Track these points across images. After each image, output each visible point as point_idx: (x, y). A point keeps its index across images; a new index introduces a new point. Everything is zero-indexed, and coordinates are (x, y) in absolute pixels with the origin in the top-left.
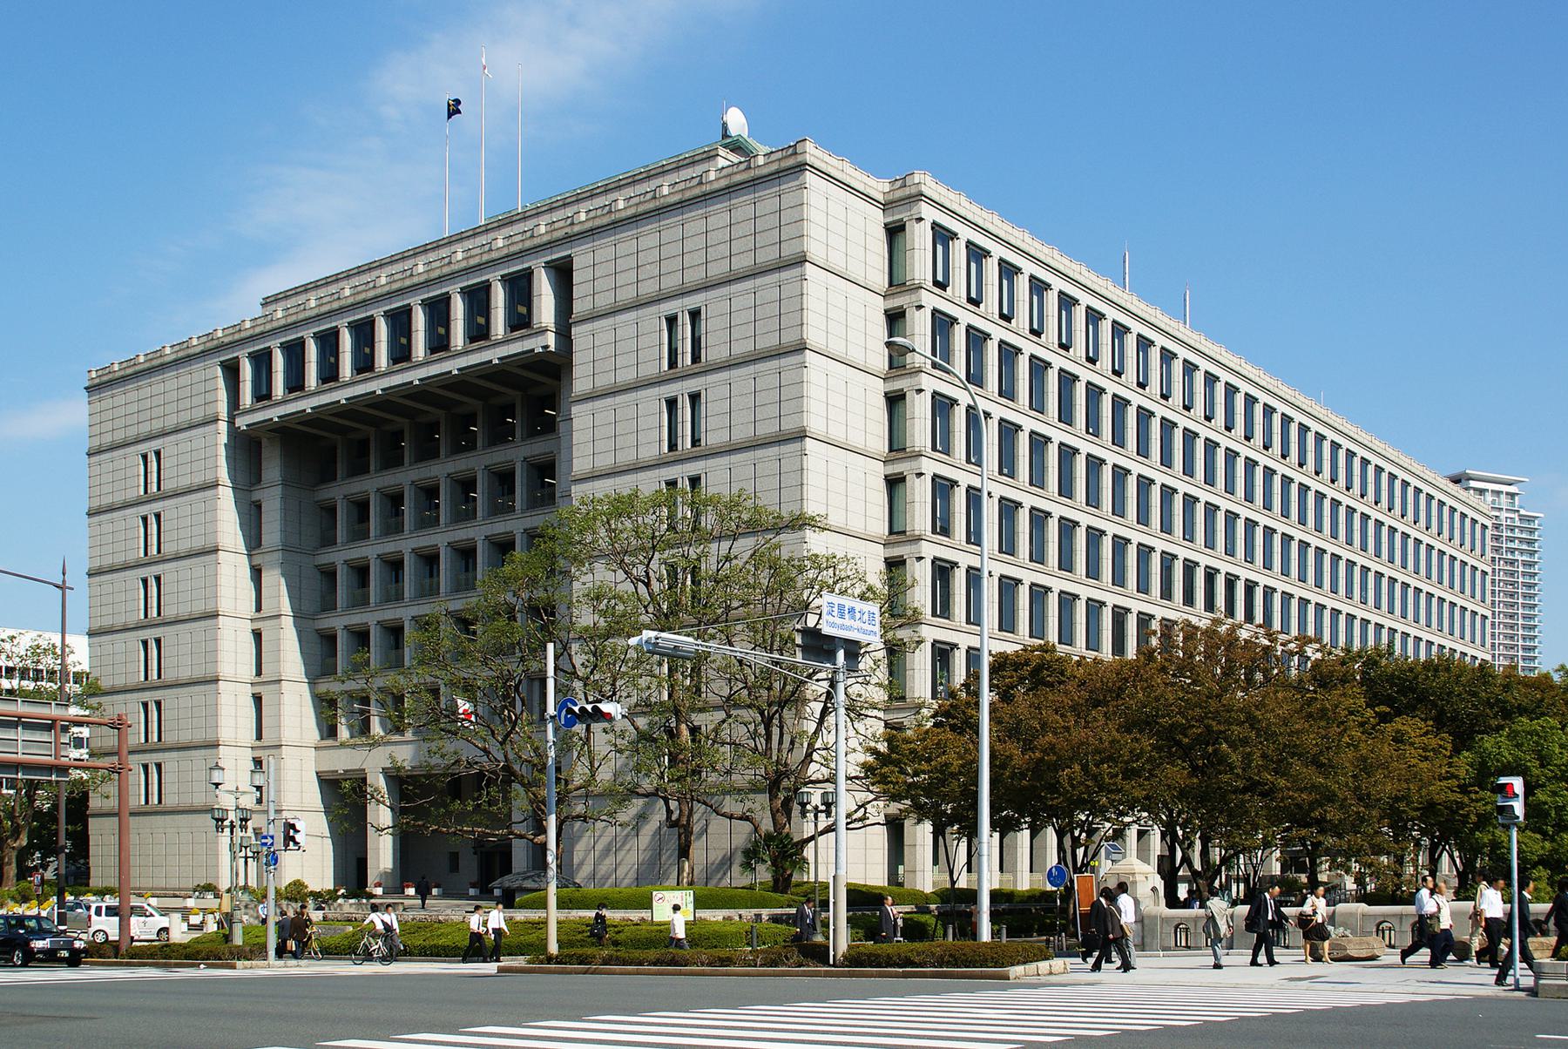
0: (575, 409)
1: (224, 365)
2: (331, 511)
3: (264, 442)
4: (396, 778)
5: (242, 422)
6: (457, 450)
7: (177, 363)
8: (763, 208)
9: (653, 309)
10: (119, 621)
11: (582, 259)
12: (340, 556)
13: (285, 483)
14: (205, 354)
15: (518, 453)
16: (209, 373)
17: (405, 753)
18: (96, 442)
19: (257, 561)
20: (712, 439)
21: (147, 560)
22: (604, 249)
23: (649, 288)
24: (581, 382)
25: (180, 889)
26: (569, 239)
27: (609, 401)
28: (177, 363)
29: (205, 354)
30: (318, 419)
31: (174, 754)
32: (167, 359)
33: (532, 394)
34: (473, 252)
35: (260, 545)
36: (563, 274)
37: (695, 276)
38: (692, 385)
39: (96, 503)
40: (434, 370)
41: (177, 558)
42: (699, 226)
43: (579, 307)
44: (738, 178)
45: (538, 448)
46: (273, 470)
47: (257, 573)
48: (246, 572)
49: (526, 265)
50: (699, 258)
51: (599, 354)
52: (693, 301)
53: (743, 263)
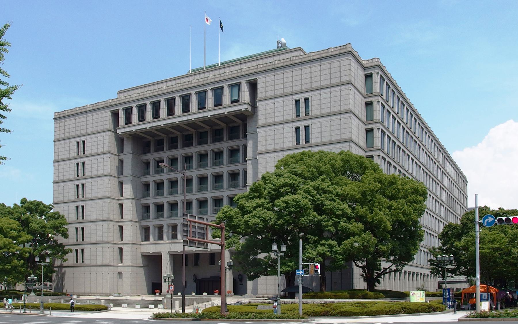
0: (258, 130)
1: (112, 112)
2: (148, 164)
3: (125, 139)
4: (175, 258)
5: (119, 131)
6: (231, 138)
7: (92, 111)
8: (94, 117)
9: (290, 97)
10: (66, 199)
11: (261, 81)
12: (152, 179)
13: (133, 153)
14: (104, 108)
15: (225, 145)
16: (106, 114)
17: (178, 247)
18: (57, 137)
19: (121, 179)
20: (87, 174)
21: (78, 178)
22: (270, 77)
23: (72, 134)
24: (261, 118)
25: (90, 293)
26: (256, 73)
27: (273, 127)
28: (92, 111)
29: (104, 108)
30: (148, 132)
31: (89, 246)
32: (88, 109)
33: (238, 126)
34: (233, 72)
35: (122, 174)
36: (253, 86)
37: (306, 87)
38: (83, 160)
39: (57, 158)
40: (140, 127)
41: (91, 178)
42: (290, 75)
43: (260, 96)
44: (324, 55)
45: (233, 144)
46: (128, 147)
47: (121, 184)
48: (117, 184)
49: (238, 81)
50: (308, 81)
51: (269, 111)
52: (83, 138)
53: (326, 83)
